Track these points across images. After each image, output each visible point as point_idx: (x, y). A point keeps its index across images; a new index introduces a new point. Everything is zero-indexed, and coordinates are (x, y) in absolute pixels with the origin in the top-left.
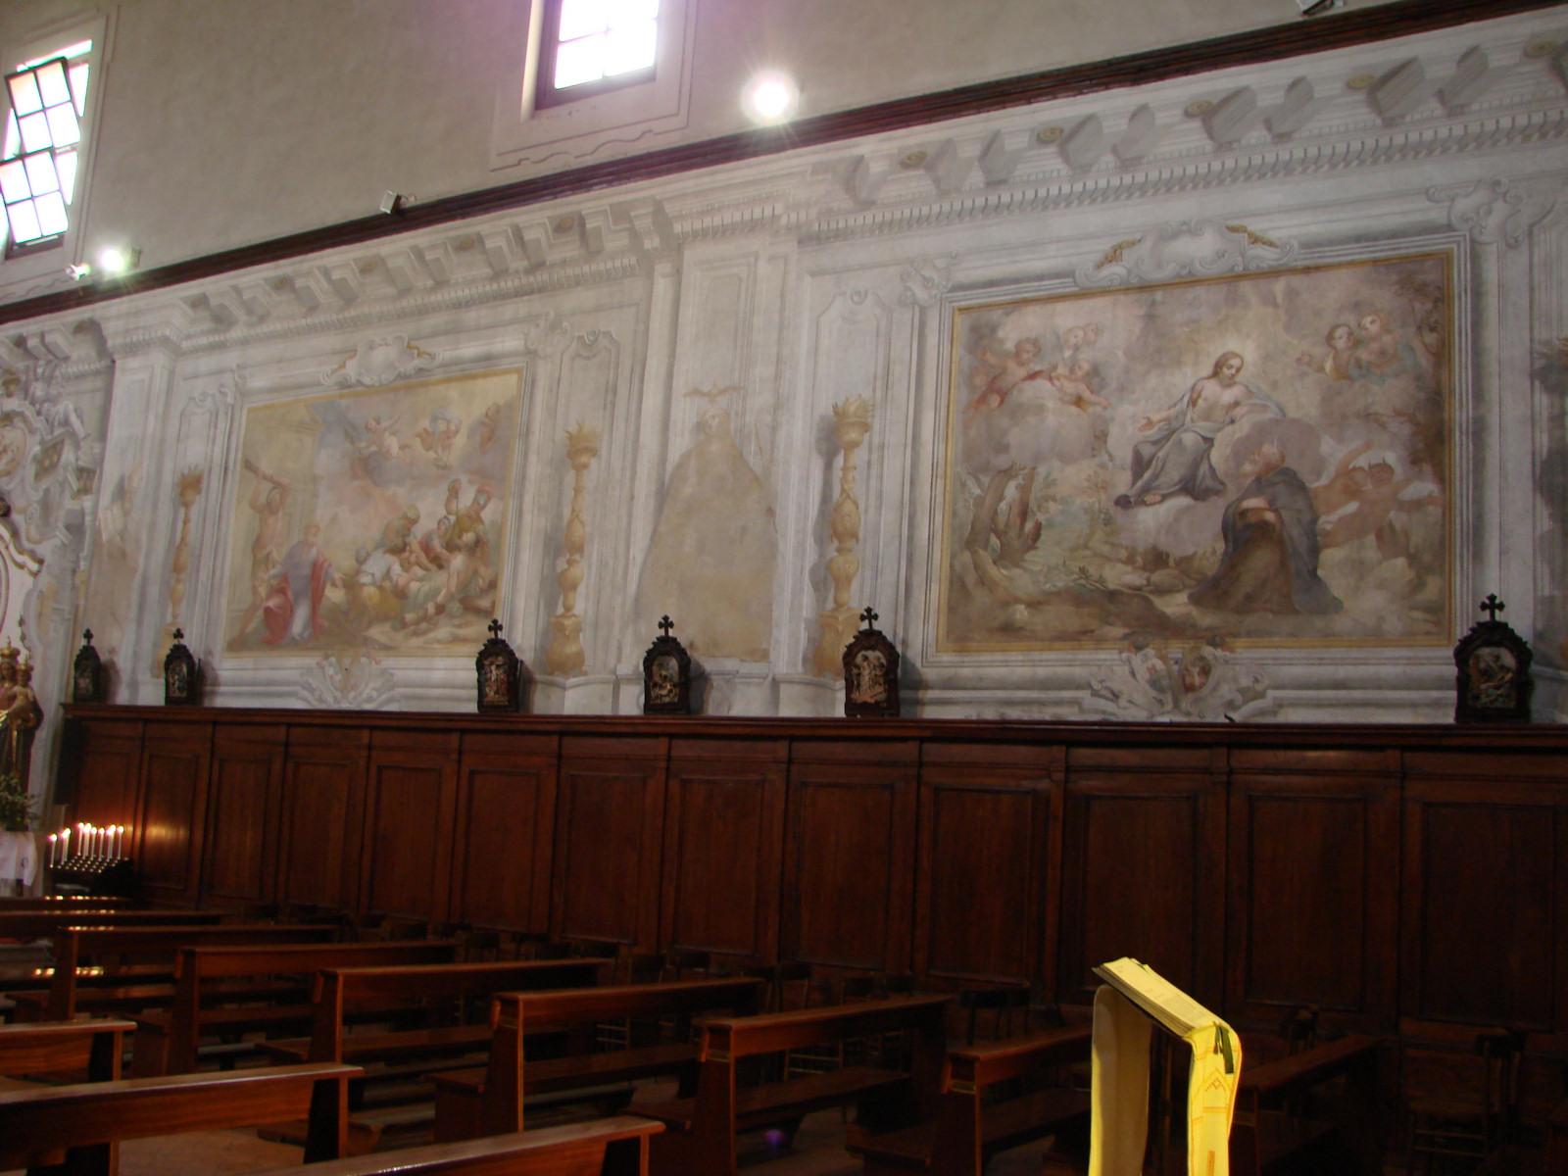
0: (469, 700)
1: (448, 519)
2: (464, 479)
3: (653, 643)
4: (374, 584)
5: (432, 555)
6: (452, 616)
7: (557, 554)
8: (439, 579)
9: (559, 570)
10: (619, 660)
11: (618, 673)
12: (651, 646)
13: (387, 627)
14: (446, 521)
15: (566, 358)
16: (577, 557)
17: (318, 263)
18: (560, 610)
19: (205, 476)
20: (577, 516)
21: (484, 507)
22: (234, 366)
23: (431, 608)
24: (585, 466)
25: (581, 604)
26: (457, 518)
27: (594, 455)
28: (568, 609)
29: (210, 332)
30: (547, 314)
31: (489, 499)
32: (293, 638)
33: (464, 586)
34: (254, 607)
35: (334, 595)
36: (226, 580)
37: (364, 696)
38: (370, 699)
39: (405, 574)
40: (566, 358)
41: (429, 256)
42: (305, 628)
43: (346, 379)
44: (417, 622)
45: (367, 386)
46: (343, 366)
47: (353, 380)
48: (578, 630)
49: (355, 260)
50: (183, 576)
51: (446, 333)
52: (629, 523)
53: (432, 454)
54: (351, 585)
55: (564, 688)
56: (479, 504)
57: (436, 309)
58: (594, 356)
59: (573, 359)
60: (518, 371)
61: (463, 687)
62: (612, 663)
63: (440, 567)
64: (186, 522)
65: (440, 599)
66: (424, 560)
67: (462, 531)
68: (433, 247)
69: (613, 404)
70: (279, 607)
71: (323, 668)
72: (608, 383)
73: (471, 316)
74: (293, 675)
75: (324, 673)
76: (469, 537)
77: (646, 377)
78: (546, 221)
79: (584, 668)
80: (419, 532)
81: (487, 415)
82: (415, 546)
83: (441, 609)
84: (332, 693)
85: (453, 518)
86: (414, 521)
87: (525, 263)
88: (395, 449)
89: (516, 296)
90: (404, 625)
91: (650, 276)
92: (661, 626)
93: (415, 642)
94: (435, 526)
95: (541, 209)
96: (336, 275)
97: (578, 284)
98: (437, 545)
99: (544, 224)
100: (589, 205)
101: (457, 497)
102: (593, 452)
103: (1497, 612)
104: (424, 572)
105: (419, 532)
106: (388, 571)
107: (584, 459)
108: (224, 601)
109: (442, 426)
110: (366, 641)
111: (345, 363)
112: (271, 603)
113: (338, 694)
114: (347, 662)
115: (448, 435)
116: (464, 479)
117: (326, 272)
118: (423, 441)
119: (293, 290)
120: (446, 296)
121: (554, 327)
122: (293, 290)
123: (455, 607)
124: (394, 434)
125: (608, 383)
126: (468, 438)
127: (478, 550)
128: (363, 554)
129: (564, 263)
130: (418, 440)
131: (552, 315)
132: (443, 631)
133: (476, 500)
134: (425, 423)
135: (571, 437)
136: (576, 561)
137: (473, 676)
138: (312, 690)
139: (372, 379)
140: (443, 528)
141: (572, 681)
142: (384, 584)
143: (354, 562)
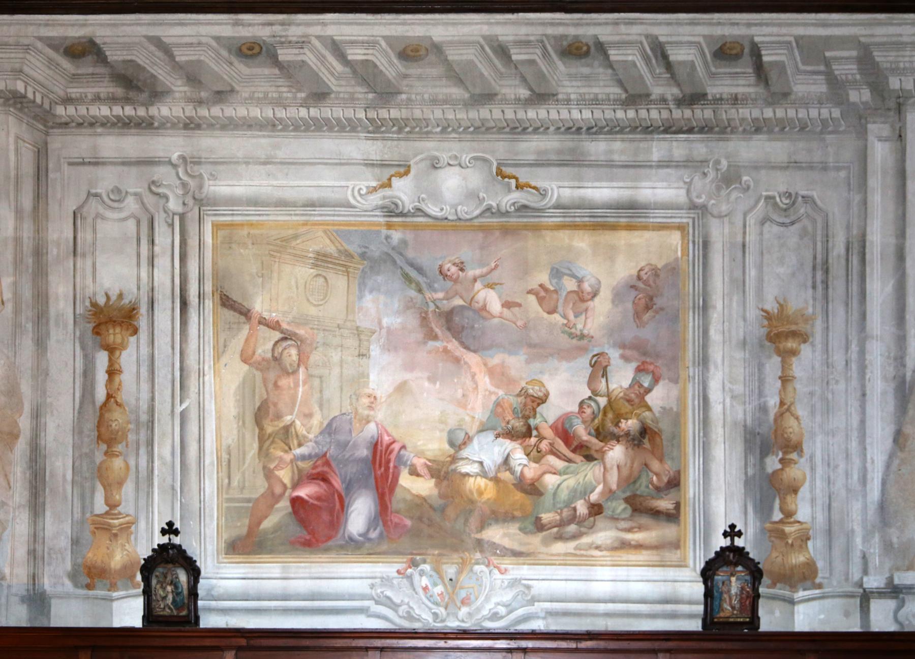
0: (691, 616)
1: (596, 401)
2: (614, 355)
3: (153, 550)
4: (484, 474)
5: (575, 443)
6: (614, 519)
7: (765, 451)
8: (590, 473)
9: (770, 470)
10: (865, 572)
11: (865, 586)
12: (150, 553)
13: (513, 529)
14: (593, 404)
15: (751, 220)
16: (794, 456)
17: (331, 31)
18: (777, 516)
19: (143, 309)
20: (788, 410)
21: (648, 391)
22: (175, 157)
23: (582, 508)
24: (794, 353)
25: (804, 510)
26: (609, 402)
27: (805, 341)
28: (788, 514)
29: (113, 100)
30: (717, 162)
31: (656, 380)
32: (351, 539)
33: (629, 481)
34: (272, 498)
35: (415, 486)
36: (210, 458)
37: (485, 612)
38: (495, 616)
39: (534, 465)
40: (751, 220)
41: (517, 55)
42: (372, 524)
43: (396, 205)
44: (562, 524)
45: (436, 218)
46: (388, 185)
47: (409, 207)
48: (805, 538)
49: (709, 38)
50: (120, 448)
51: (562, 164)
52: (863, 422)
53: (557, 318)
54: (443, 472)
55: (792, 602)
56: (641, 386)
57: (540, 129)
58: (793, 223)
59: (762, 223)
60: (681, 228)
61: (690, 602)
62: (856, 575)
63: (589, 458)
64: (112, 372)
65: (594, 497)
66: (561, 446)
67: (618, 418)
68: (524, 43)
69: (826, 283)
70: (318, 498)
71: (410, 578)
72: (815, 258)
73: (597, 148)
74: (361, 587)
75: (412, 584)
76: (630, 424)
77: (868, 257)
78: (701, 40)
79: (818, 580)
80: (550, 413)
81: (639, 278)
82: (548, 433)
83: (596, 509)
84: (430, 609)
85: (603, 401)
86: (542, 400)
87: (676, 91)
88: (495, 304)
89: (666, 131)
90: (539, 526)
91: (862, 133)
92: (725, 534)
93: (559, 547)
94: (576, 409)
95: (692, 23)
96: (356, 54)
97: (758, 130)
98: (581, 431)
99: (699, 43)
100: (766, 30)
101: (605, 374)
102: (803, 337)
103: (736, 538)
104: (566, 464)
105: (550, 413)
106: (506, 460)
107: (790, 344)
108: (210, 486)
109: (570, 285)
110: (480, 545)
111: (390, 179)
112: (303, 492)
113: (441, 611)
114: (450, 571)
115: (582, 298)
116: (614, 355)
117: (337, 49)
118: (540, 300)
119: (274, 61)
120: (554, 115)
121: (730, 179)
122: (274, 61)
123: (620, 507)
124: (491, 286)
125: (815, 258)
126: (613, 302)
127: (646, 441)
128: (461, 436)
129: (735, 100)
130: (532, 298)
131: (724, 164)
132: (604, 535)
133: (635, 383)
134: (543, 277)
135: (768, 316)
136: (792, 461)
137: (699, 589)
138: (394, 607)
139: (442, 209)
140: (588, 411)
141: (801, 594)
142: (499, 475)
143: (447, 446)
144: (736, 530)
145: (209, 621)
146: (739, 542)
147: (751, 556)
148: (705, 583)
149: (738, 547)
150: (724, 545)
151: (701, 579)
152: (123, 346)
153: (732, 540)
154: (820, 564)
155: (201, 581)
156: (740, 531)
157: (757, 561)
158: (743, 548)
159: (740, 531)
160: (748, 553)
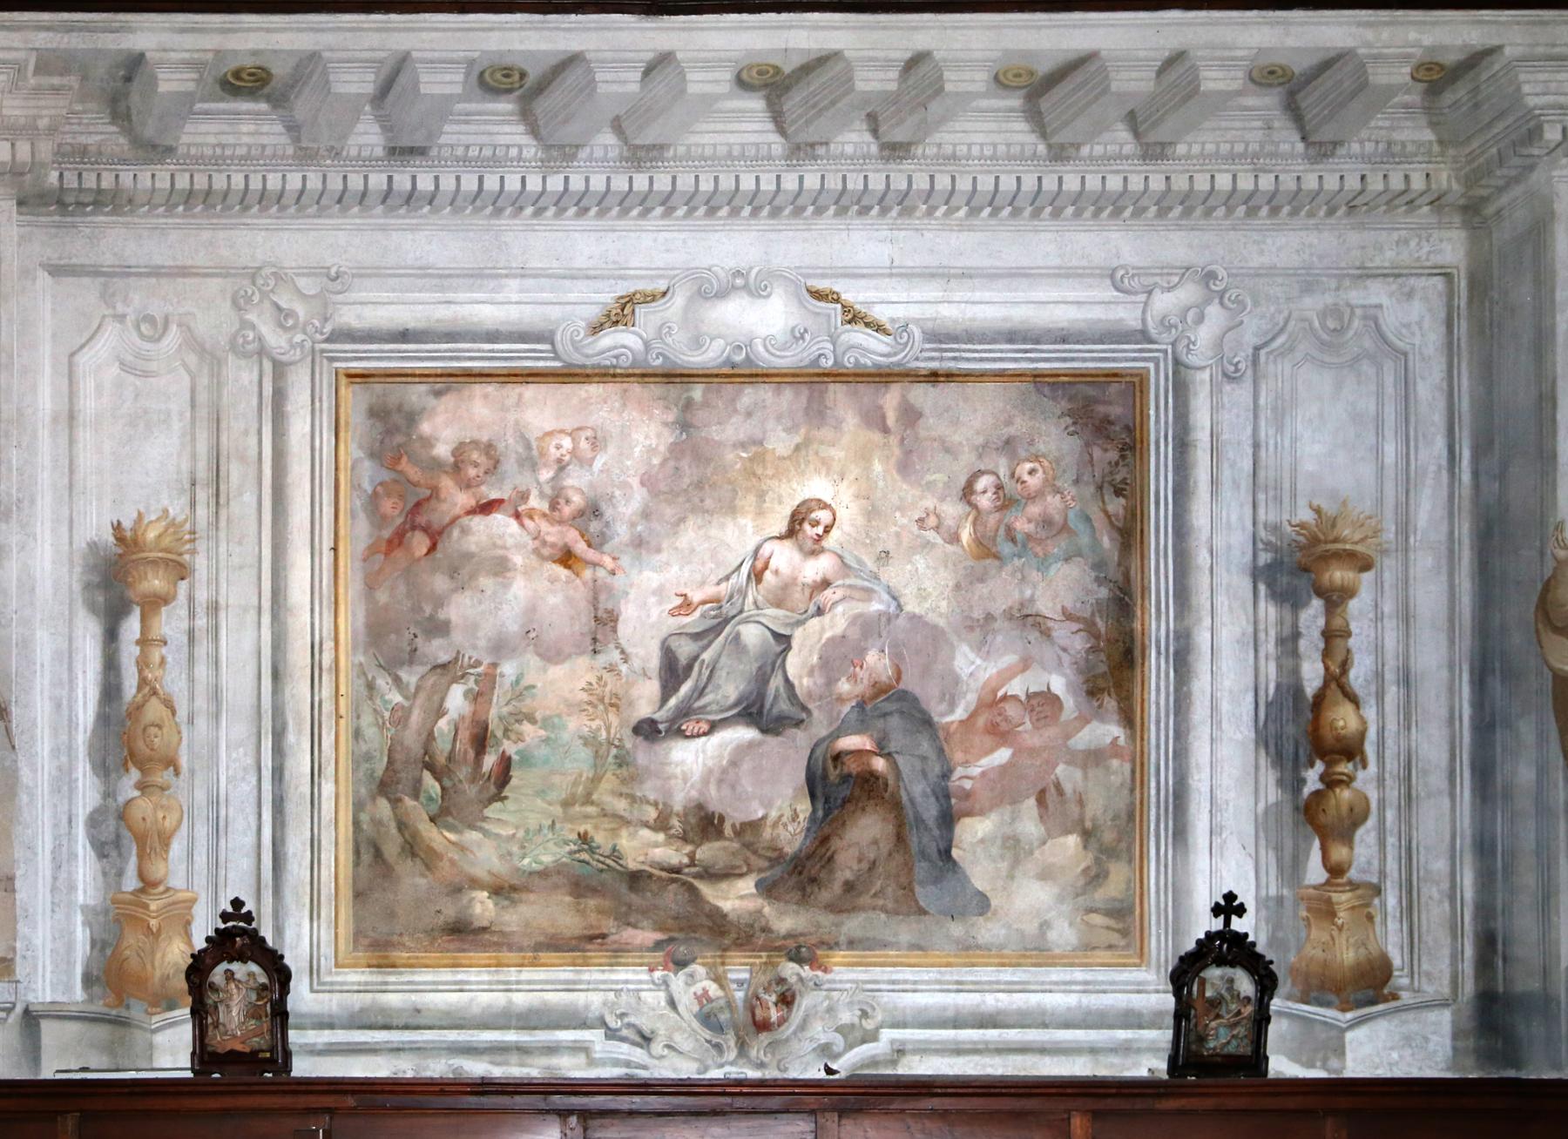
0: (1153, 1049)
3: (193, 956)
12: (204, 945)
64: (1333, 636)
92: (1217, 910)
103: (1234, 918)
144: (244, 910)
145: (302, 1067)
146: (1238, 924)
147: (1259, 949)
148: (1177, 993)
149: (1237, 933)
150: (1214, 929)
151: (1170, 988)
152: (1348, 592)
153: (1227, 922)
154: (1397, 962)
156: (1242, 905)
157: (1268, 958)
158: (1246, 935)
159: (1242, 905)
160: (1253, 944)
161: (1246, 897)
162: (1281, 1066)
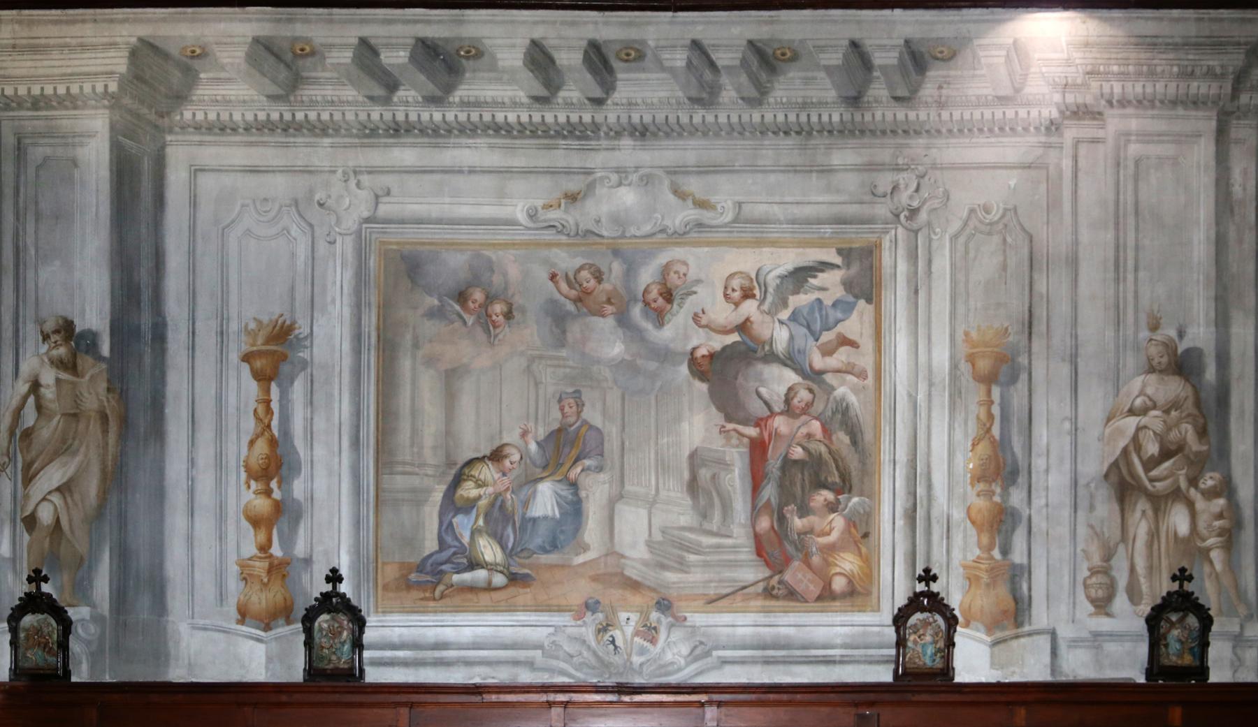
92: (328, 579)
103: (1186, 583)
145: (373, 675)
155: (366, 630)
158: (1193, 593)
161: (344, 572)
162: (1217, 676)
